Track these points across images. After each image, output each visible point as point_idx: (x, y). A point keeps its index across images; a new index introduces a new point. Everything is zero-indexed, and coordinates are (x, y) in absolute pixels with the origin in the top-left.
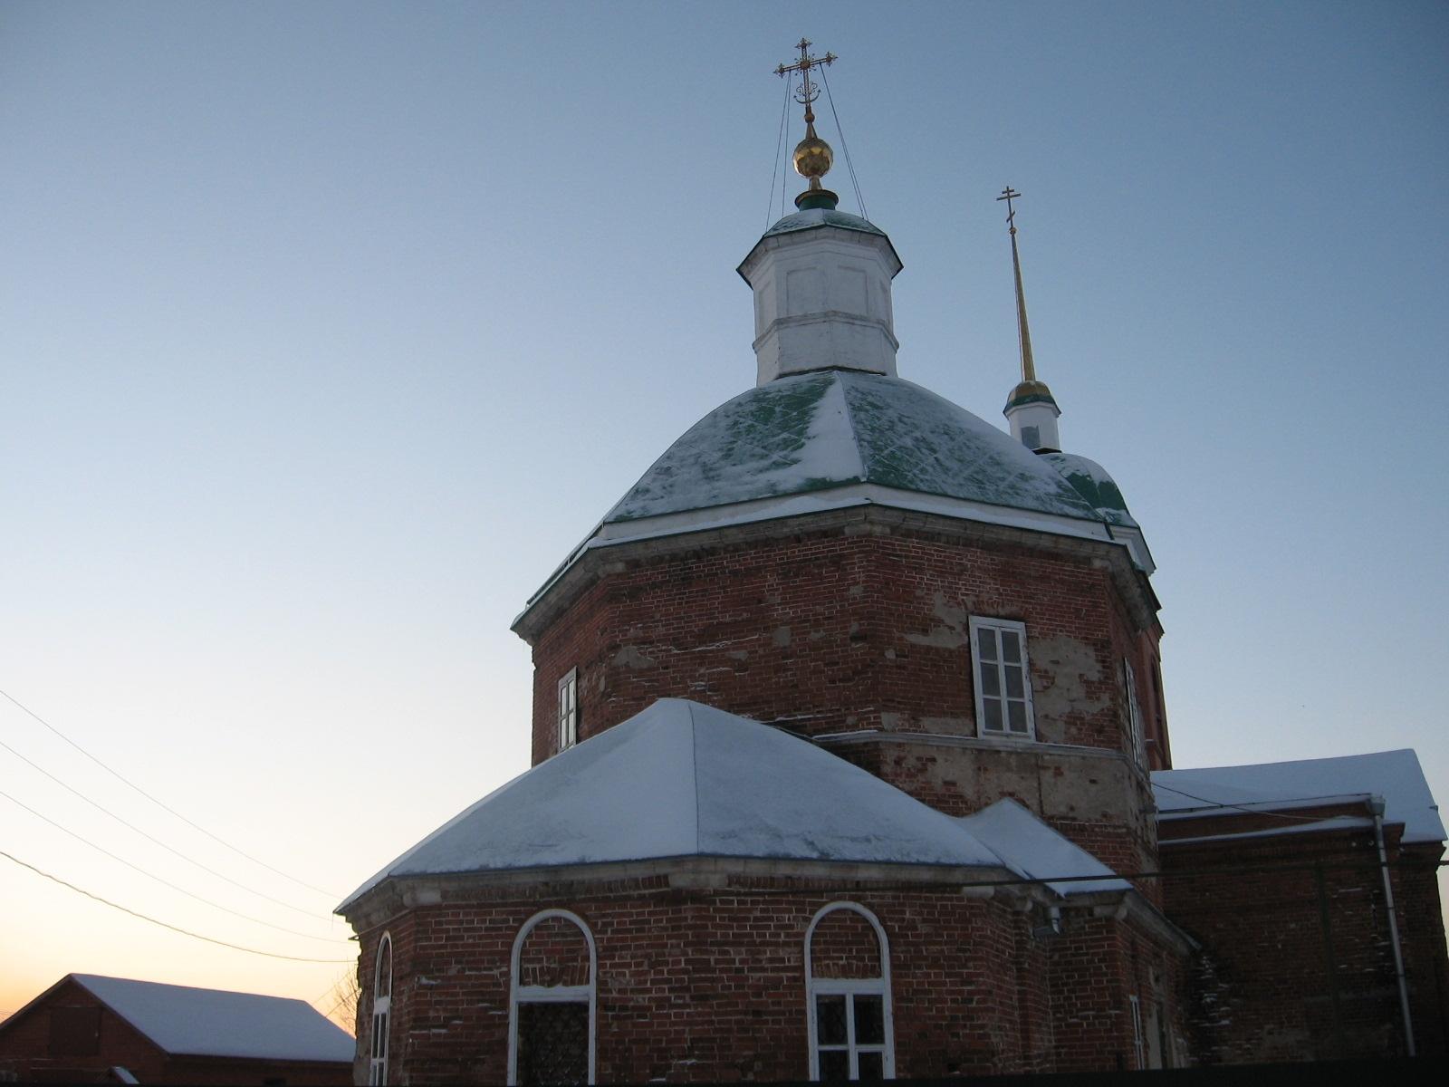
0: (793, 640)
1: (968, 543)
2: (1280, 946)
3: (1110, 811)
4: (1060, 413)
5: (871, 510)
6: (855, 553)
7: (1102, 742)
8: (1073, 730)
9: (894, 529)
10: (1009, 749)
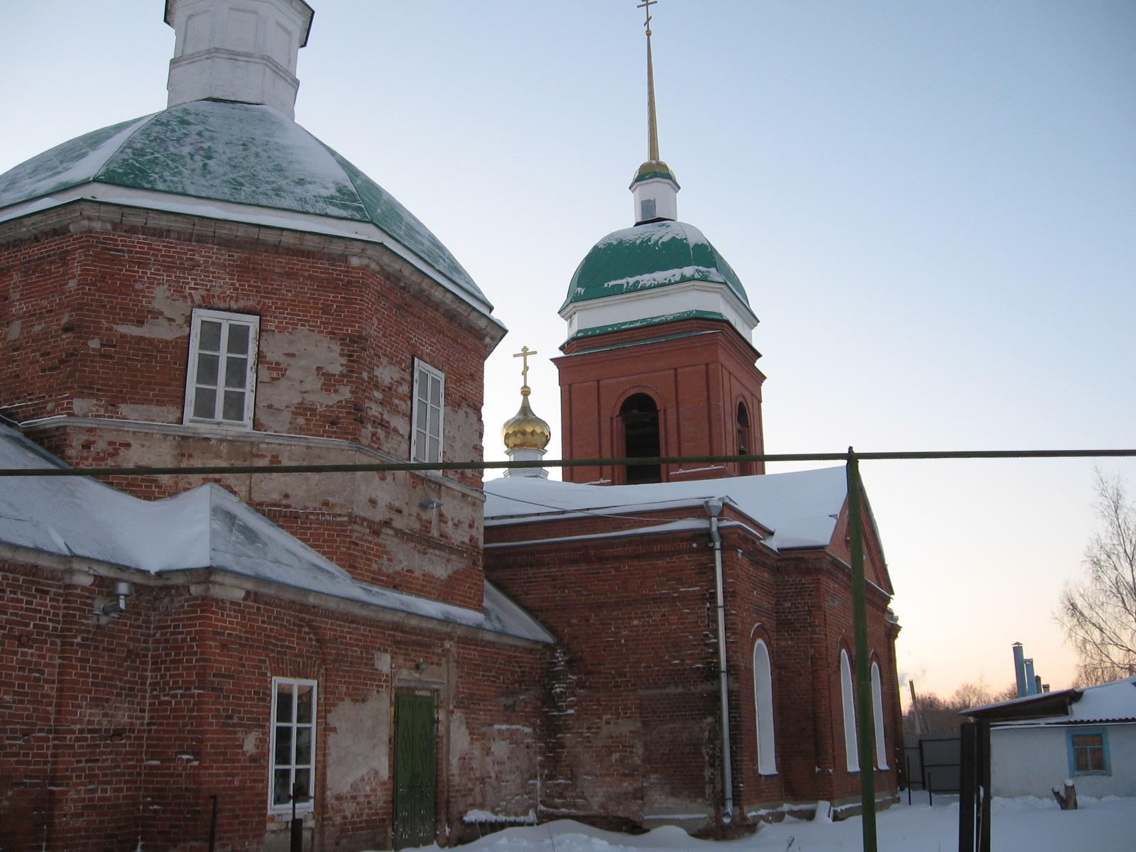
0: (22, 333)
1: (202, 239)
2: (623, 641)
3: (331, 500)
4: (680, 188)
5: (84, 205)
6: (77, 249)
7: (335, 432)
8: (301, 421)
9: (115, 226)
10: (219, 437)
